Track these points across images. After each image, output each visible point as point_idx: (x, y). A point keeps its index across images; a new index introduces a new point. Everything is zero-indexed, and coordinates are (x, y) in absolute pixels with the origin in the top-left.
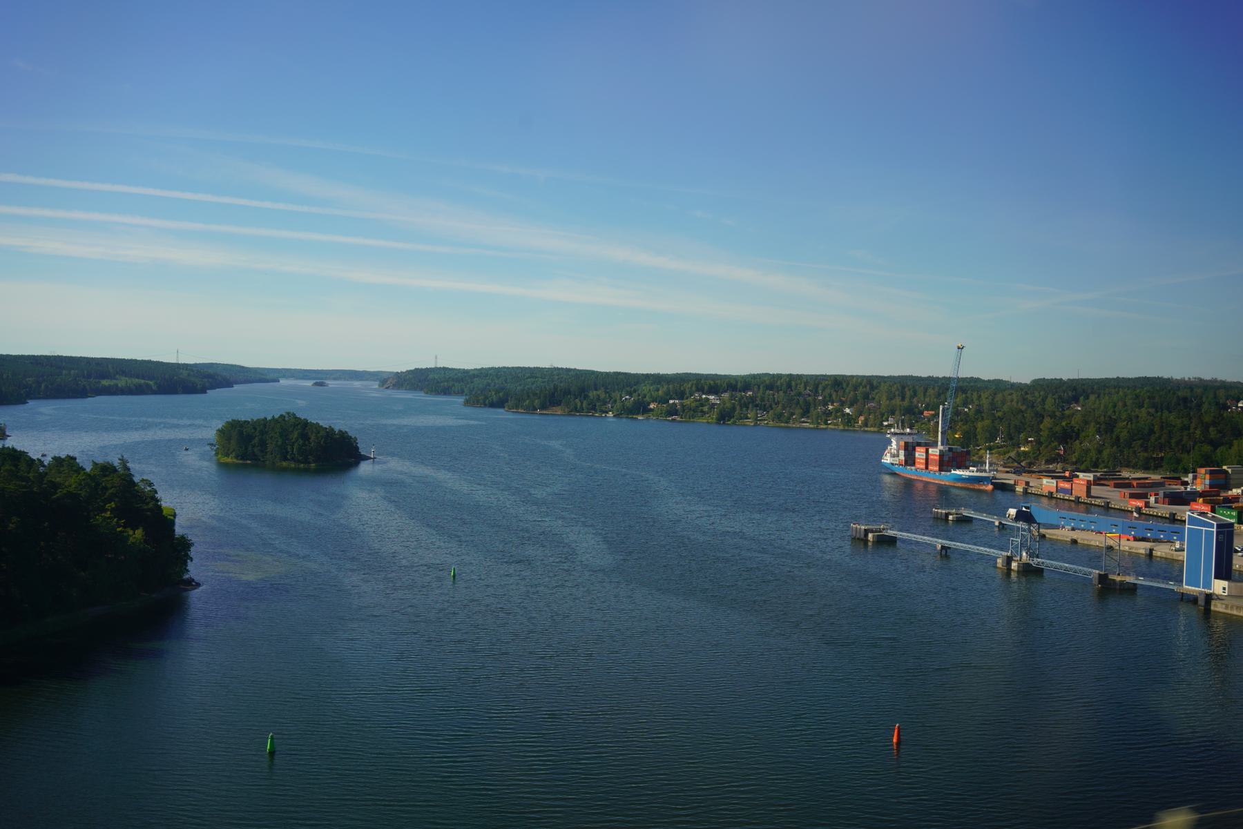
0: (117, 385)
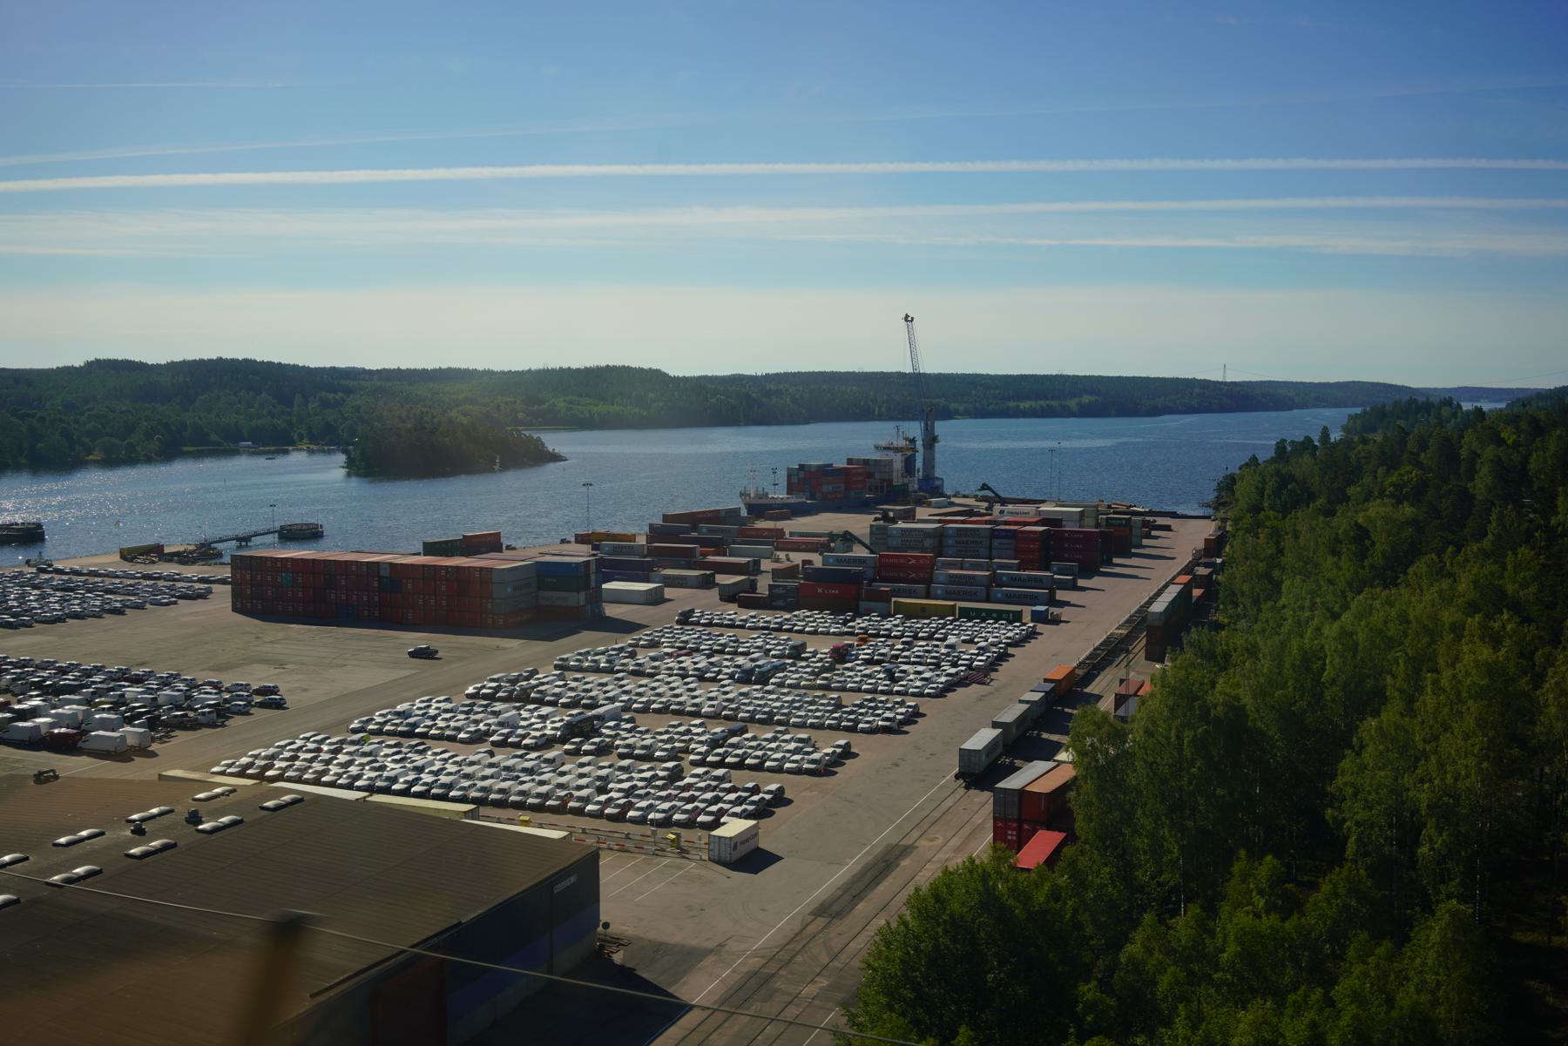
0: (1018, 406)
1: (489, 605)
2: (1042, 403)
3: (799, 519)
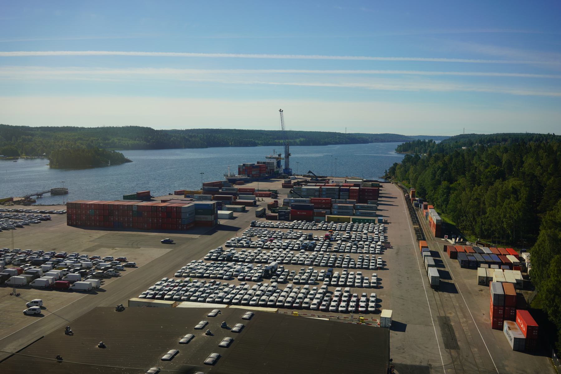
0: (279, 142)
1: (180, 221)
3: (248, 184)
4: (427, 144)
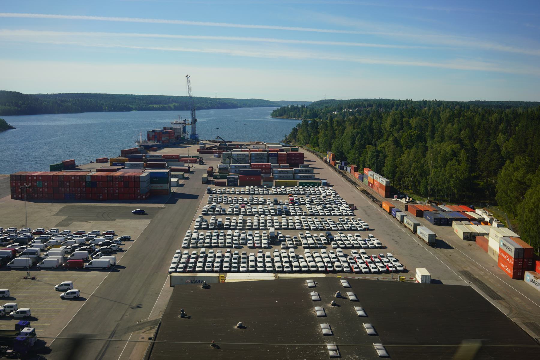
0: (153, 106)
1: (138, 191)
2: (161, 105)
4: (301, 109)
